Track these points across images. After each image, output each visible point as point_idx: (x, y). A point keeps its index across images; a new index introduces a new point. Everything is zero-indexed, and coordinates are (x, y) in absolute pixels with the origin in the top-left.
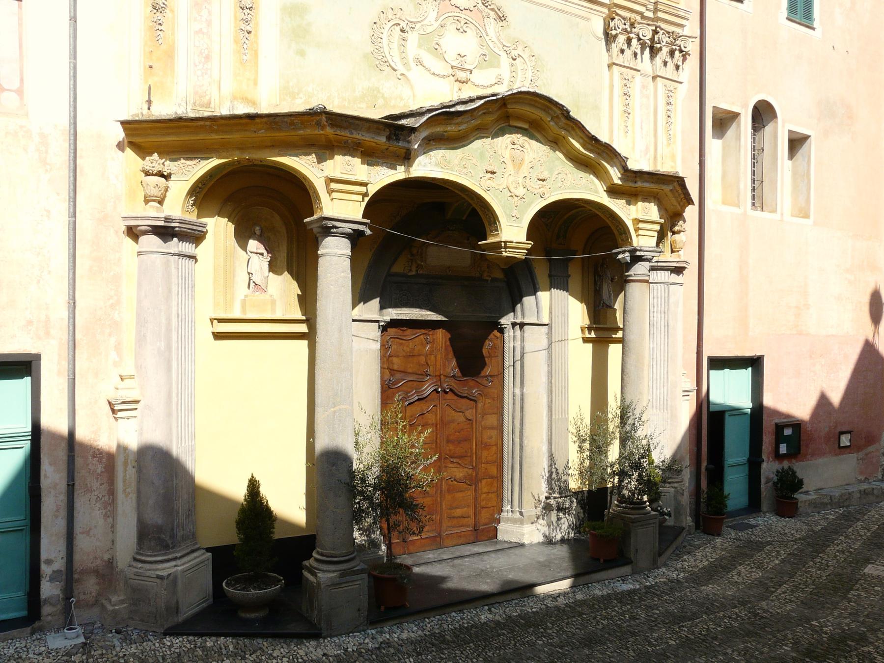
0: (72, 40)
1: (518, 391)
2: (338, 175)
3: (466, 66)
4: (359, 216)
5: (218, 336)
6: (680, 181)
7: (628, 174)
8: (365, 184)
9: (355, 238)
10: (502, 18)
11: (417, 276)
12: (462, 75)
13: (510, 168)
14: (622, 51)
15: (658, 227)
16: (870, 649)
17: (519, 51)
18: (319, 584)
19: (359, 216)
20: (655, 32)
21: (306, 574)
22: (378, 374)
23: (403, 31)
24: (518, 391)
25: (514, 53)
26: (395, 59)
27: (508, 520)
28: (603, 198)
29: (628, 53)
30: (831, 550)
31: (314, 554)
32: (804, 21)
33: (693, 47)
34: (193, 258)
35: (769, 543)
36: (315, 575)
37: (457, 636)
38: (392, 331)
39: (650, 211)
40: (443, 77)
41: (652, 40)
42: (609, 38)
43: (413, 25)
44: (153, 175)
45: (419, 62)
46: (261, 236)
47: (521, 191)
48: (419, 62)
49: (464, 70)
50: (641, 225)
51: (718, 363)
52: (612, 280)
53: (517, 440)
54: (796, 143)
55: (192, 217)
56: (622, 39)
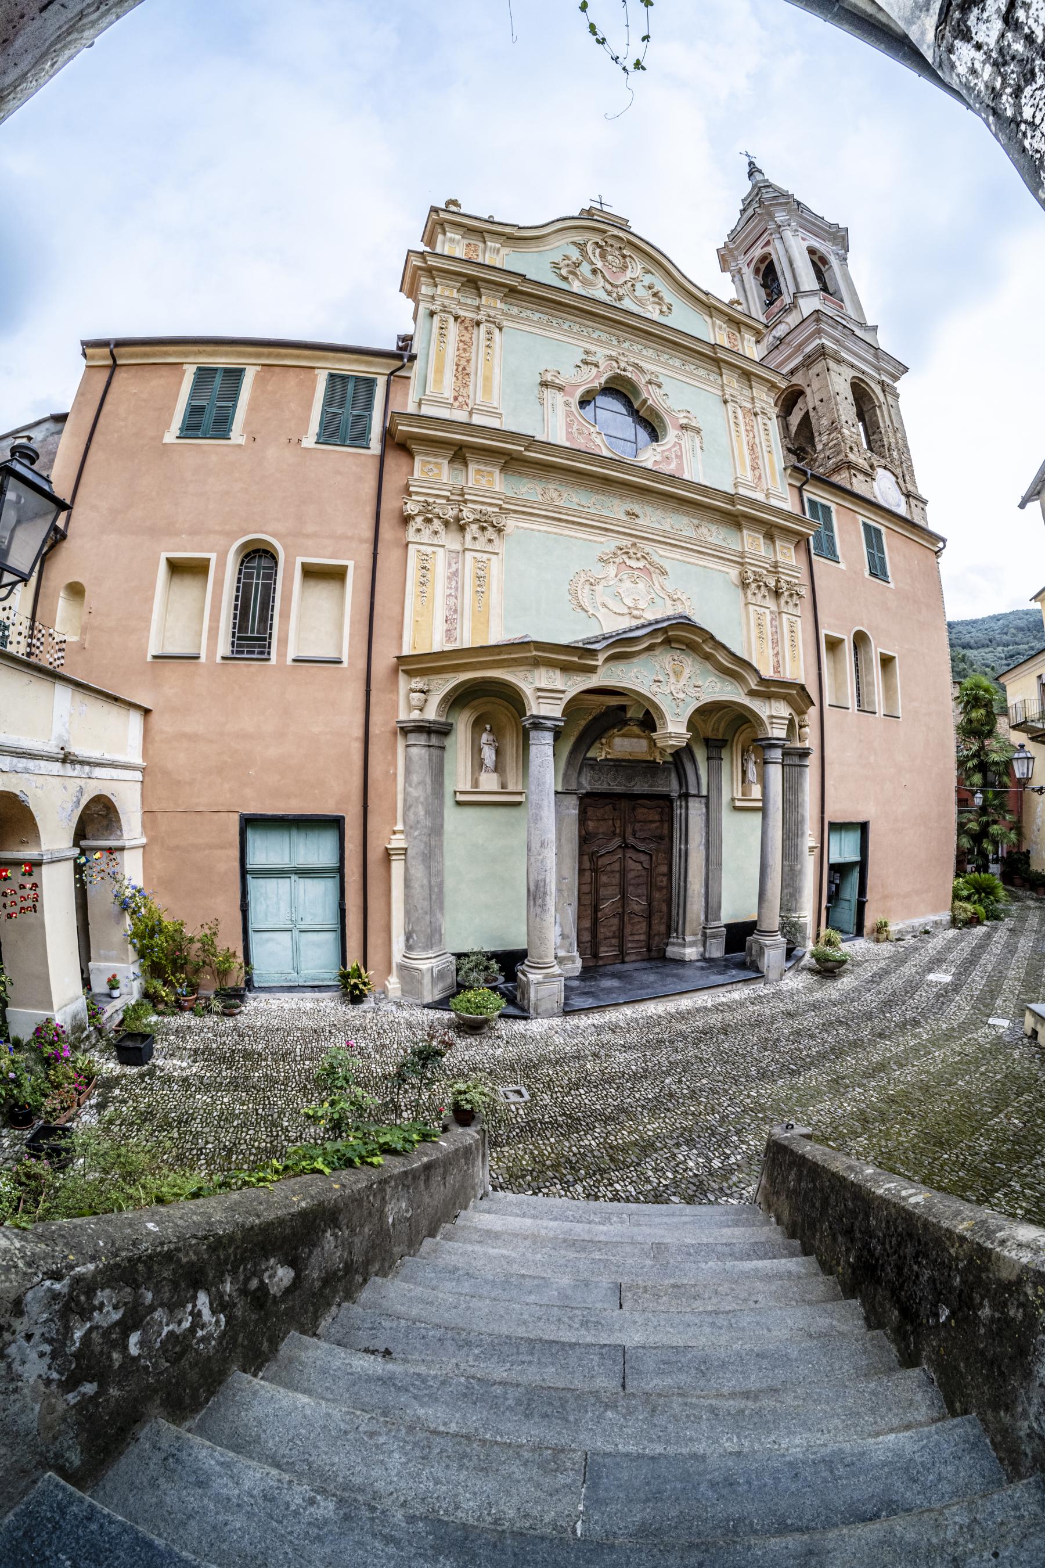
0: (104, 25)
1: (683, 847)
2: (543, 686)
3: (639, 607)
4: (559, 715)
5: (459, 804)
6: (802, 688)
7: (762, 681)
8: (563, 692)
9: (558, 734)
10: (664, 573)
11: (606, 759)
12: (635, 613)
13: (673, 679)
14: (787, 603)
15: (787, 722)
16: (921, 1030)
17: (679, 595)
18: (528, 982)
19: (559, 715)
20: (778, 581)
21: (520, 975)
22: (577, 832)
23: (591, 584)
24: (683, 847)
25: (675, 597)
26: (586, 603)
27: (673, 944)
28: (746, 701)
29: (760, 596)
30: (909, 964)
31: (526, 962)
32: (881, 577)
33: (805, 591)
34: (409, 378)
35: (867, 961)
36: (525, 975)
37: (628, 1024)
38: (588, 801)
39: (783, 710)
40: (623, 615)
41: (776, 586)
42: (744, 585)
43: (598, 581)
44: (416, 692)
45: (605, 606)
46: (490, 731)
47: (682, 696)
48: (605, 606)
49: (639, 609)
50: (774, 720)
51: (837, 827)
52: (755, 763)
53: (682, 884)
54: (887, 661)
55: (443, 719)
56: (754, 585)
